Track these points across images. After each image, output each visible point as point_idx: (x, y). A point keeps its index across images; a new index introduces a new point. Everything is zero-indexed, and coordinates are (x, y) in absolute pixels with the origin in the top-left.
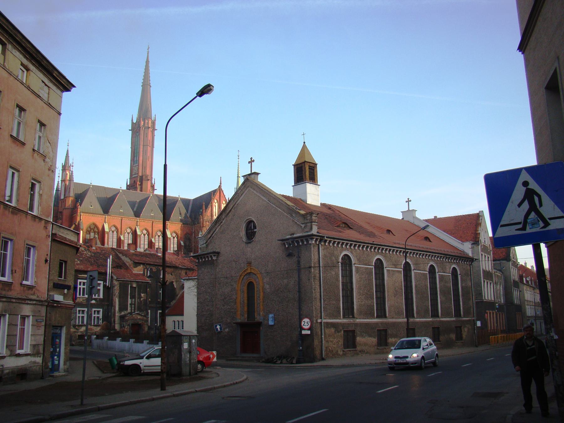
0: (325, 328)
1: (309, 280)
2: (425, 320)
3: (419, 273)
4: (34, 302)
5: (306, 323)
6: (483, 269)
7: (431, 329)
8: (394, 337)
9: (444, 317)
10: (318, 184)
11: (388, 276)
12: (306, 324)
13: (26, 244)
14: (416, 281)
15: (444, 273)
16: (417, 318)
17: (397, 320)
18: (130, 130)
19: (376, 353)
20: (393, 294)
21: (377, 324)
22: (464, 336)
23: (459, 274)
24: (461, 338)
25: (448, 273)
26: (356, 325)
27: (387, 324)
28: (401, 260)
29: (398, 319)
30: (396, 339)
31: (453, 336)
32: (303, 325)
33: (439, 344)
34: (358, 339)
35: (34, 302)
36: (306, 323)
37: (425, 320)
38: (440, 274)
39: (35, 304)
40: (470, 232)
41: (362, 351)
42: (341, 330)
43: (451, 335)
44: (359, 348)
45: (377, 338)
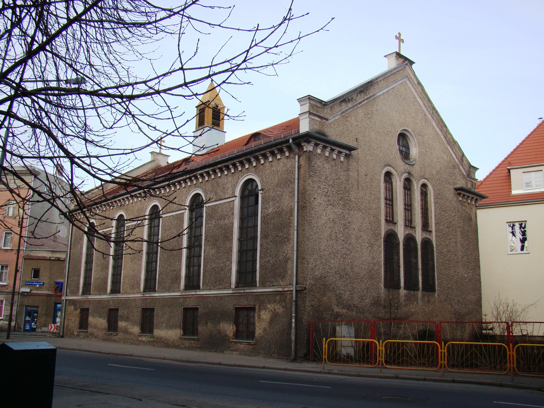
0: (68, 306)
2: (168, 294)
3: (170, 216)
4: (6, 293)
6: (319, 144)
7: (181, 310)
8: (126, 321)
9: (208, 288)
10: (224, 131)
13: (522, 252)
14: (164, 232)
16: (203, 290)
17: (129, 296)
19: (104, 340)
20: (130, 260)
21: (108, 301)
22: (258, 331)
24: (251, 335)
26: (90, 301)
27: (120, 300)
28: (145, 207)
29: (129, 295)
30: (126, 323)
31: (229, 328)
33: (194, 339)
34: (90, 319)
35: (6, 293)
37: (168, 294)
39: (6, 294)
41: (92, 334)
42: (78, 309)
43: (222, 325)
44: (90, 330)
45: (106, 320)
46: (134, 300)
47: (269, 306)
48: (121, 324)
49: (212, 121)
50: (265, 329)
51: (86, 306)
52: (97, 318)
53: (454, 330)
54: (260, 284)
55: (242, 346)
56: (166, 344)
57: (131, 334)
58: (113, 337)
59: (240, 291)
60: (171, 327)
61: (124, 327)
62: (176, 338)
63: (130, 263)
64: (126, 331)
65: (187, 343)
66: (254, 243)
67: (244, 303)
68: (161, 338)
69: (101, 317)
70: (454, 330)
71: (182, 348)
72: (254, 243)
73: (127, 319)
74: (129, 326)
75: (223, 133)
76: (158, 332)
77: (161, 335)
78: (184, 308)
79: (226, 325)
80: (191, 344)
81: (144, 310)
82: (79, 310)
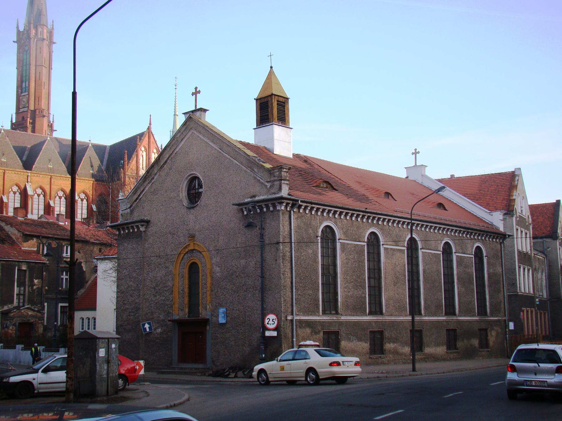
1: (276, 260)
5: (271, 320)
8: (394, 342)
9: (463, 315)
10: (290, 127)
11: (386, 257)
12: (271, 322)
15: (464, 253)
18: (14, 42)
21: (370, 322)
22: (491, 343)
23: (486, 256)
24: (487, 346)
25: (470, 254)
26: (341, 323)
27: (383, 323)
28: (404, 235)
30: (395, 344)
31: (475, 342)
32: (268, 324)
36: (271, 320)
38: (458, 256)
40: (502, 198)
46: (402, 322)
47: (495, 328)
48: (389, 346)
49: (277, 107)
50: (494, 342)
51: (333, 329)
52: (355, 342)
53: (247, 317)
54: (459, 311)
55: (483, 353)
56: (435, 358)
57: (401, 354)
58: (380, 360)
59: (482, 318)
60: (438, 345)
61: (393, 348)
62: (444, 353)
63: (393, 285)
64: (395, 352)
65: (452, 356)
66: (369, 266)
67: (484, 326)
68: (431, 354)
69: (360, 340)
70: (247, 317)
71: (448, 360)
72: (369, 266)
73: (395, 340)
74: (399, 347)
75: (290, 129)
76: (428, 350)
77: (431, 352)
78: (446, 329)
79: (474, 340)
80: (454, 356)
81: (413, 331)
82: (322, 334)
